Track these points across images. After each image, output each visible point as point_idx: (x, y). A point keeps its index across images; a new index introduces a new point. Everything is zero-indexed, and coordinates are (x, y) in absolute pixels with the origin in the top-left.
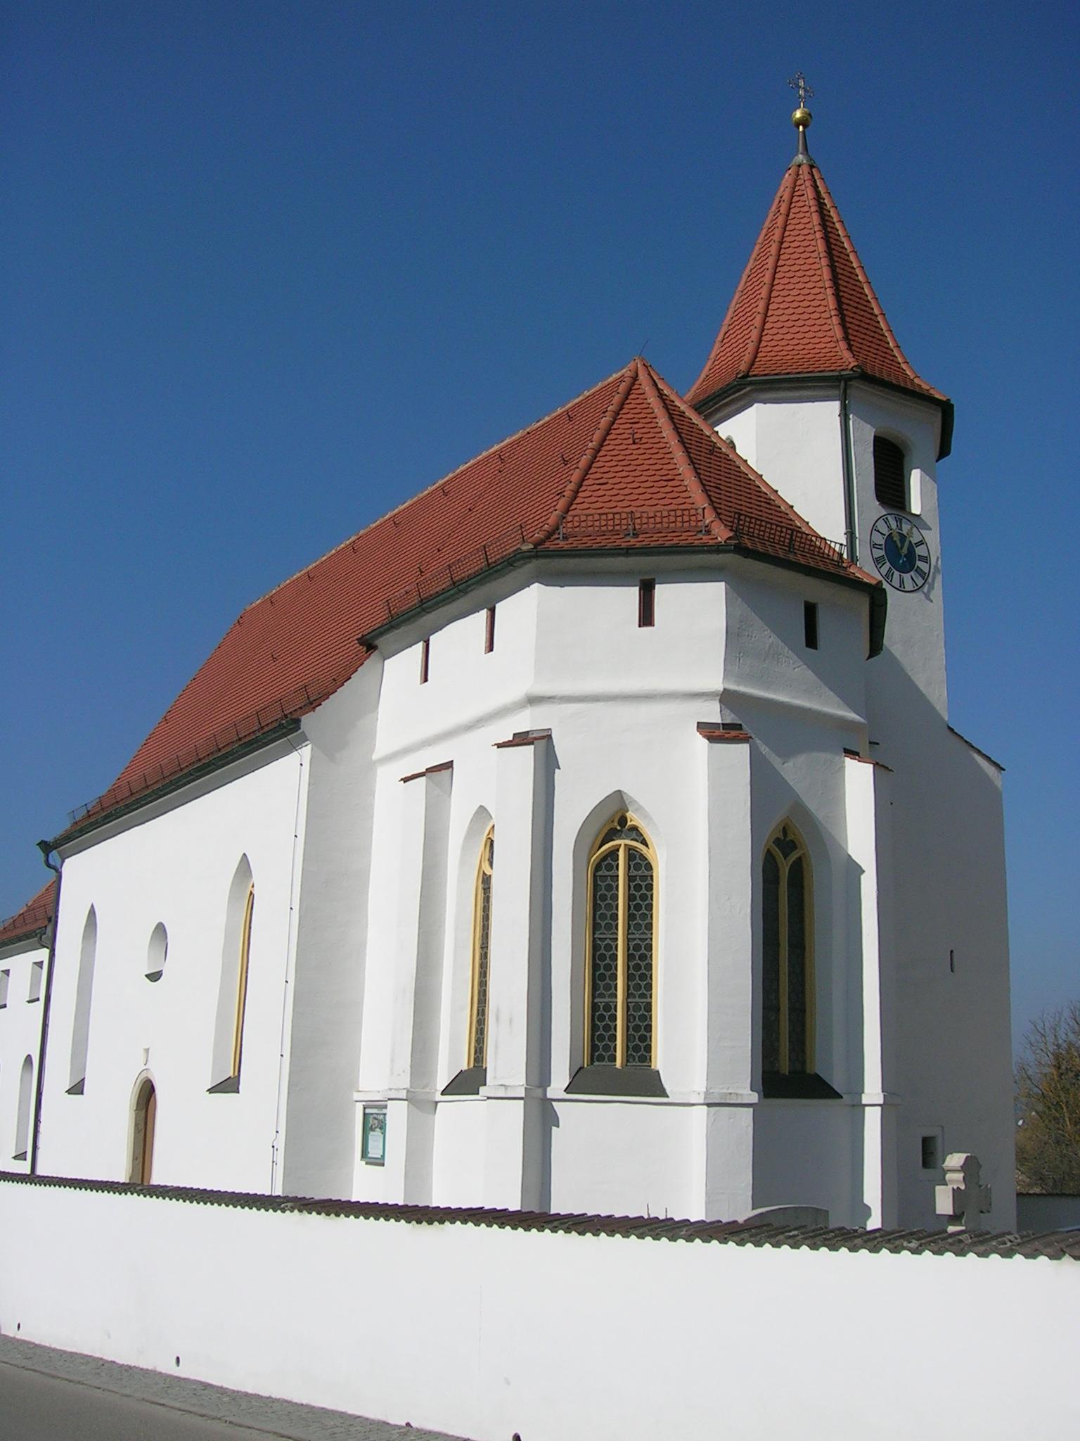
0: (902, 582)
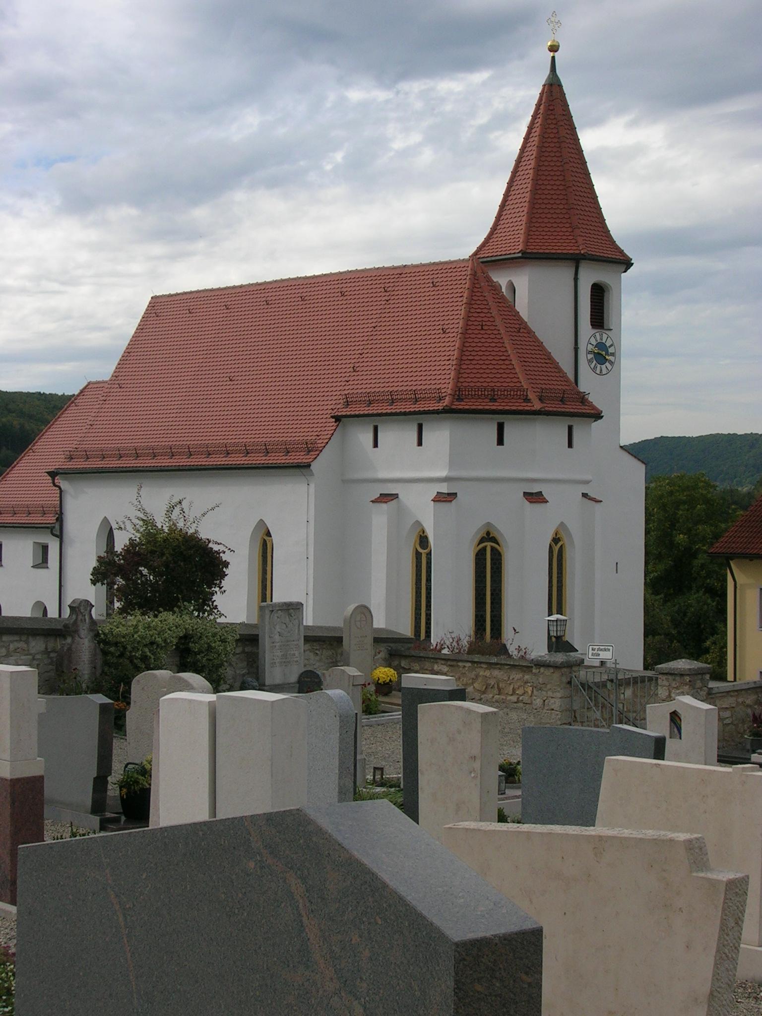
0: (595, 367)
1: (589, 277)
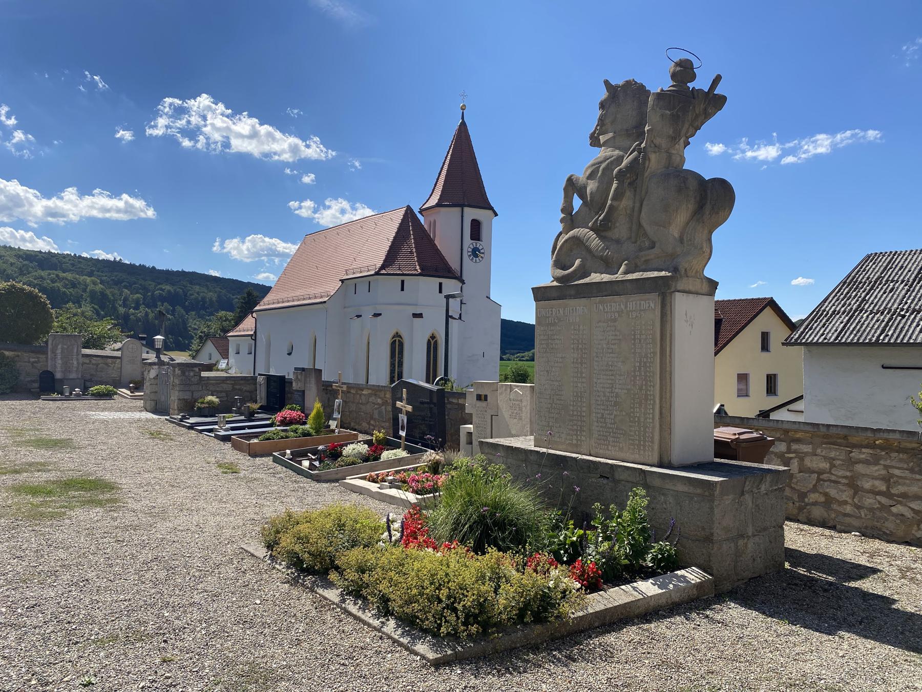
1: (471, 213)
